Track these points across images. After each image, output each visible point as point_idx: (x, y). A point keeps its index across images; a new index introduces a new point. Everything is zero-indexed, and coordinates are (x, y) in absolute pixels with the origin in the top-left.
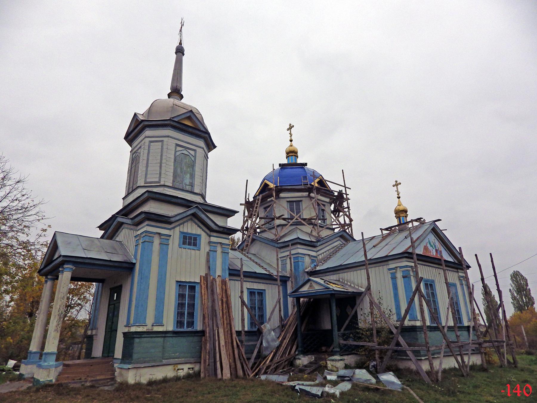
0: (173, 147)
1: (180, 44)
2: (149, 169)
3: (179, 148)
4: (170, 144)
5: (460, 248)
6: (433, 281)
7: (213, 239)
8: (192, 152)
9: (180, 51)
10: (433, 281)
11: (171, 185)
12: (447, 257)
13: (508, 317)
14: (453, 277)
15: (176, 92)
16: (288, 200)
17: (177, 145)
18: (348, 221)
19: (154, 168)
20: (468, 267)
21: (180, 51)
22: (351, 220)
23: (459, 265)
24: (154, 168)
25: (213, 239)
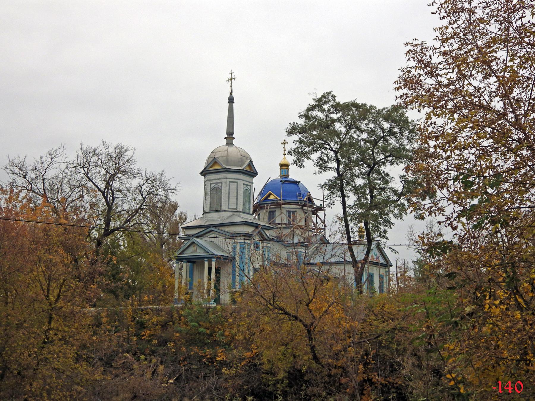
0: (242, 186)
1: (231, 94)
2: (230, 200)
3: (245, 186)
4: (241, 183)
5: (406, 44)
6: (373, 274)
7: (265, 244)
8: (249, 187)
9: (231, 100)
10: (373, 274)
11: (241, 210)
12: (382, 261)
13: (231, 266)
14: (383, 271)
15: (230, 137)
16: (288, 209)
17: (244, 184)
18: (323, 227)
19: (233, 200)
20: (391, 266)
21: (231, 100)
22: (325, 226)
23: (387, 265)
24: (233, 200)
25: (265, 244)
